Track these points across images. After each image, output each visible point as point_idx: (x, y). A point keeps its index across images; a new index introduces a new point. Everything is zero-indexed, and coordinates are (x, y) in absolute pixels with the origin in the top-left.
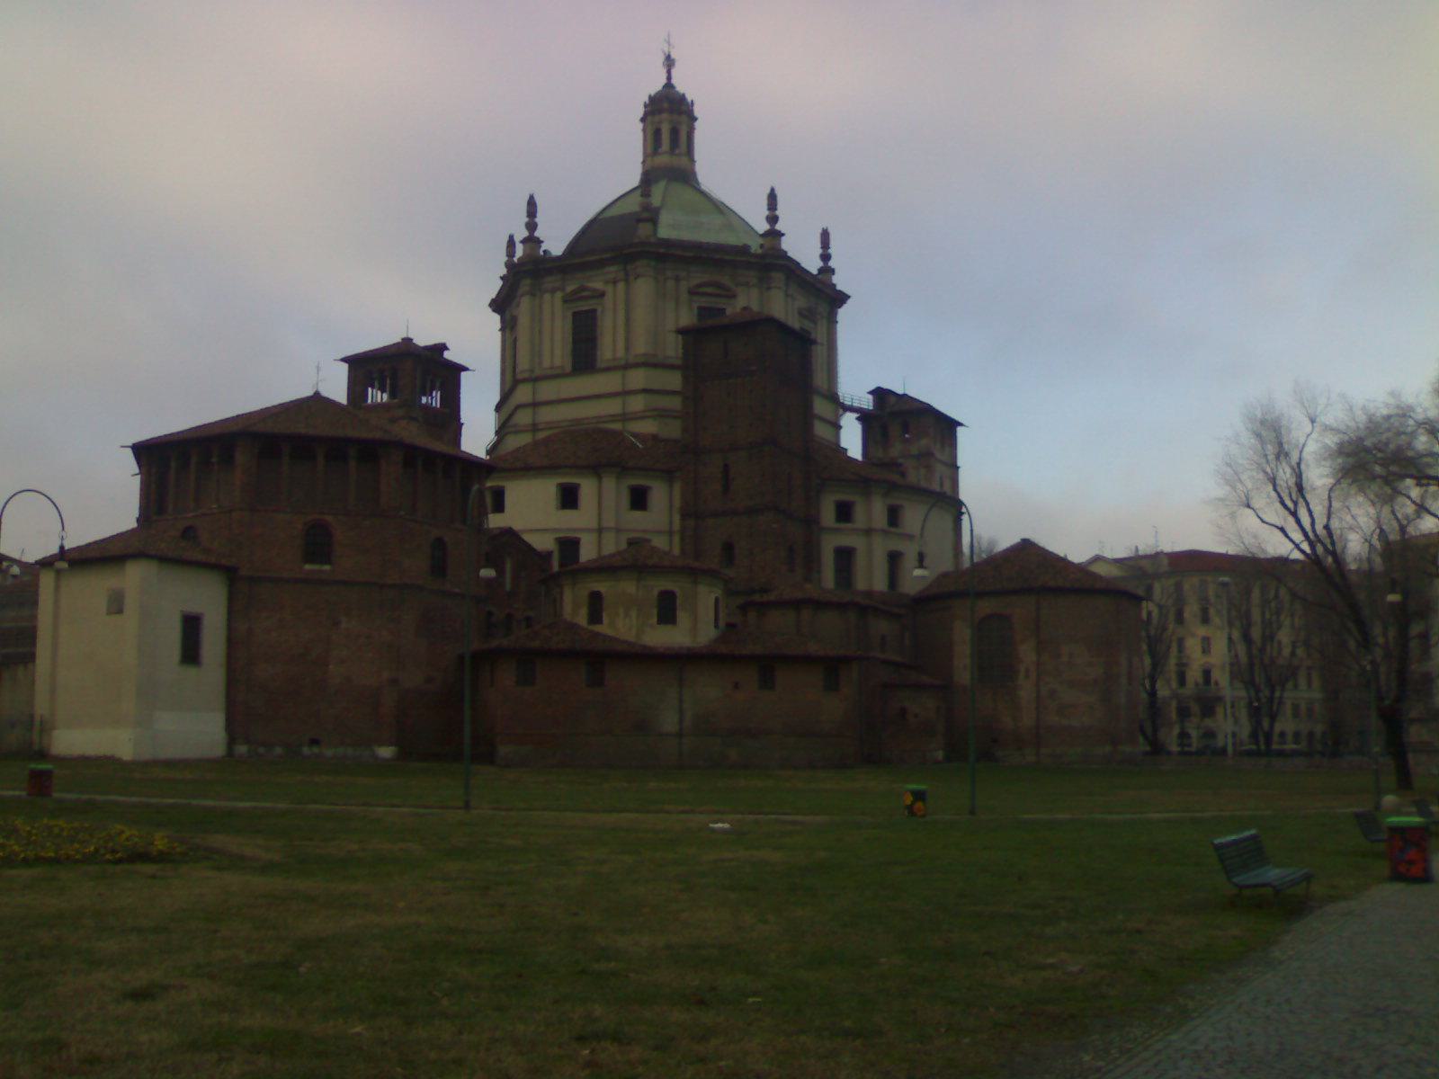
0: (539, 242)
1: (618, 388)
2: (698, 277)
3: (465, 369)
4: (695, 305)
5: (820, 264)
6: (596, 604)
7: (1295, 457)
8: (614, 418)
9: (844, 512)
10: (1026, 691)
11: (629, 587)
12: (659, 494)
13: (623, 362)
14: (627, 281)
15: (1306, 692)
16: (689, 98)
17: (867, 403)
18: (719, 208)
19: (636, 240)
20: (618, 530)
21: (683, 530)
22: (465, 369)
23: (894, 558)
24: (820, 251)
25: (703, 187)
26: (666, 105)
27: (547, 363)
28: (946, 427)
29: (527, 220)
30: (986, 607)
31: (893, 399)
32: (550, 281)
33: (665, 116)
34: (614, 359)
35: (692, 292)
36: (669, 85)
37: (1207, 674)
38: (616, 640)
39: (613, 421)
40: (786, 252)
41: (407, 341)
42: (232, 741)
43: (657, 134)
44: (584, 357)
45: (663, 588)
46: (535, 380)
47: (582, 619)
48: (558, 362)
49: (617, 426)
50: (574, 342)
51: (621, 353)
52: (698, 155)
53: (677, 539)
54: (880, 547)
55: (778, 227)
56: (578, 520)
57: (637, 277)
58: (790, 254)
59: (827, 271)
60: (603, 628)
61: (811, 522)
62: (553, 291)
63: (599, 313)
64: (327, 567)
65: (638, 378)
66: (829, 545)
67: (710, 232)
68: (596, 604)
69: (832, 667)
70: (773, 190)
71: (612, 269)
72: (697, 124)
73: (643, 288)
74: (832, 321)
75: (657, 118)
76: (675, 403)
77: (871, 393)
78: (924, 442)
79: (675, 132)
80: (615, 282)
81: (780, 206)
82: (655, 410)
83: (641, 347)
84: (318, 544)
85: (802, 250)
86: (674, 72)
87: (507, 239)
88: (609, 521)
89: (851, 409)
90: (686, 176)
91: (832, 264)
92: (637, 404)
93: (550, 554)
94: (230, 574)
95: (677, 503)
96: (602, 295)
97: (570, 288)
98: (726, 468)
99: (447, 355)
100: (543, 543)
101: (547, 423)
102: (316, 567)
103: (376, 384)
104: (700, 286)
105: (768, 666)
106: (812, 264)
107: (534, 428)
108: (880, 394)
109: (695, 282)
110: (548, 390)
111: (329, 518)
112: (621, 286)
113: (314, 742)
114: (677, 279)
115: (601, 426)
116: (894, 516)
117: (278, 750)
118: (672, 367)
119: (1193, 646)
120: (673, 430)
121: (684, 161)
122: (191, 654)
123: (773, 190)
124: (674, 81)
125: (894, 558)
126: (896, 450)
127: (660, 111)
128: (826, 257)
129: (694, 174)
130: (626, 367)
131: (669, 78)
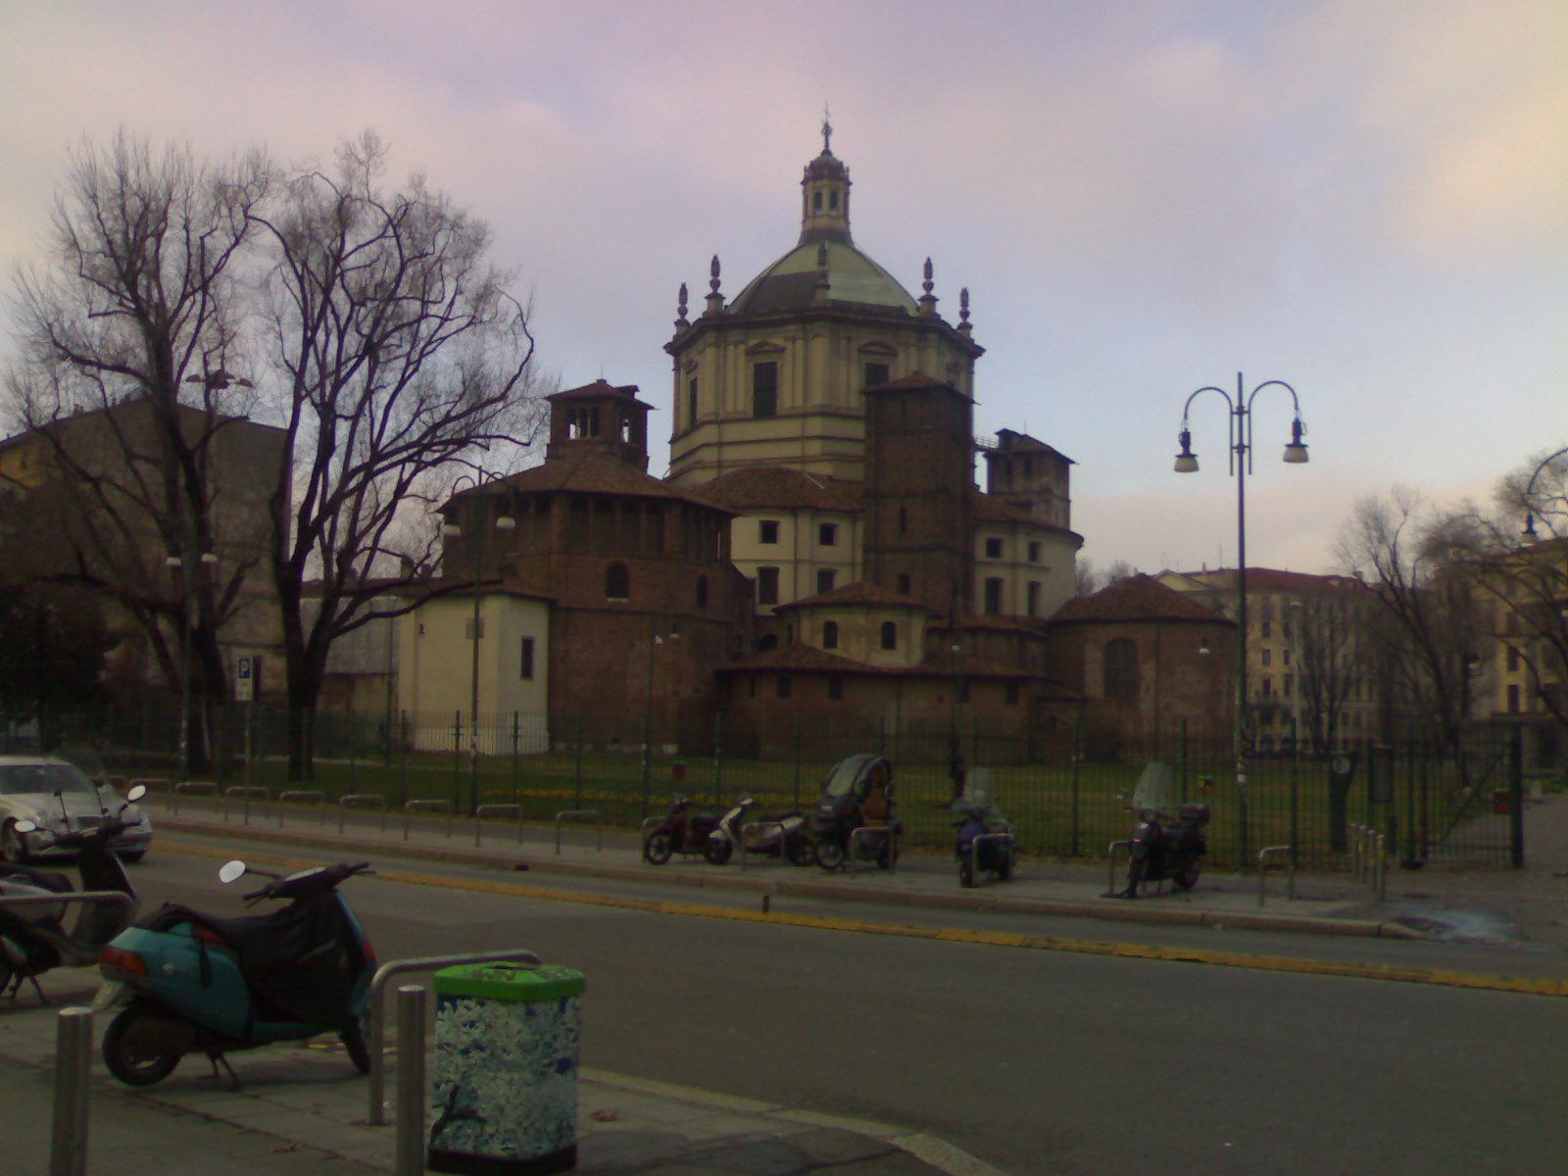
0: (721, 298)
1: (798, 434)
2: (866, 337)
3: (651, 408)
4: (864, 362)
5: (923, 293)
6: (831, 633)
7: (1391, 541)
8: (792, 460)
9: (994, 548)
10: (1146, 705)
11: (860, 619)
12: (844, 532)
13: (802, 412)
14: (805, 340)
15: (1363, 704)
16: (845, 165)
17: (993, 442)
18: (877, 271)
19: (813, 305)
20: (812, 562)
21: (865, 563)
22: (651, 408)
23: (1033, 587)
24: (960, 309)
25: (856, 247)
26: (826, 172)
27: (730, 407)
28: (1062, 464)
29: (711, 278)
30: (1114, 632)
31: (1016, 440)
32: (734, 335)
33: (825, 182)
34: (793, 408)
35: (861, 351)
36: (827, 152)
37: (1267, 683)
38: (849, 661)
39: (792, 462)
40: (939, 316)
41: (602, 382)
42: (552, 739)
43: (818, 197)
44: (765, 404)
45: (886, 621)
46: (721, 422)
47: (818, 642)
48: (741, 407)
49: (796, 467)
50: (756, 391)
51: (799, 402)
52: (852, 216)
53: (859, 569)
54: (1024, 577)
55: (934, 293)
56: (777, 553)
57: (816, 336)
58: (943, 318)
59: (966, 327)
60: (838, 651)
61: (968, 557)
62: (736, 344)
63: (778, 366)
64: (625, 600)
65: (815, 426)
66: (981, 576)
67: (870, 295)
68: (831, 633)
69: (1012, 686)
70: (929, 260)
71: (793, 327)
72: (852, 188)
73: (820, 347)
74: (970, 372)
75: (818, 183)
76: (859, 449)
77: (997, 433)
78: (1045, 480)
79: (834, 198)
80: (794, 340)
81: (935, 274)
82: (830, 454)
83: (818, 398)
84: (617, 581)
85: (948, 312)
86: (831, 139)
87: (679, 287)
88: (804, 554)
89: (981, 449)
90: (843, 237)
91: (970, 320)
92: (815, 448)
93: (754, 580)
94: (552, 606)
95: (860, 539)
96: (782, 350)
97: (752, 342)
98: (903, 511)
99: (638, 396)
100: (749, 571)
101: (733, 461)
102: (617, 600)
103: (578, 421)
104: (867, 345)
105: (966, 684)
106: (954, 321)
107: (720, 465)
108: (1006, 435)
109: (863, 342)
110: (733, 432)
111: (626, 561)
112: (800, 344)
113: (615, 741)
114: (849, 339)
115: (786, 466)
116: (1034, 551)
117: (588, 747)
118: (857, 418)
119: (1254, 658)
120: (856, 472)
121: (841, 223)
122: (527, 672)
123: (929, 260)
124: (832, 148)
125: (1033, 587)
126: (1019, 484)
127: (821, 177)
128: (965, 314)
129: (848, 233)
130: (805, 415)
131: (827, 144)
